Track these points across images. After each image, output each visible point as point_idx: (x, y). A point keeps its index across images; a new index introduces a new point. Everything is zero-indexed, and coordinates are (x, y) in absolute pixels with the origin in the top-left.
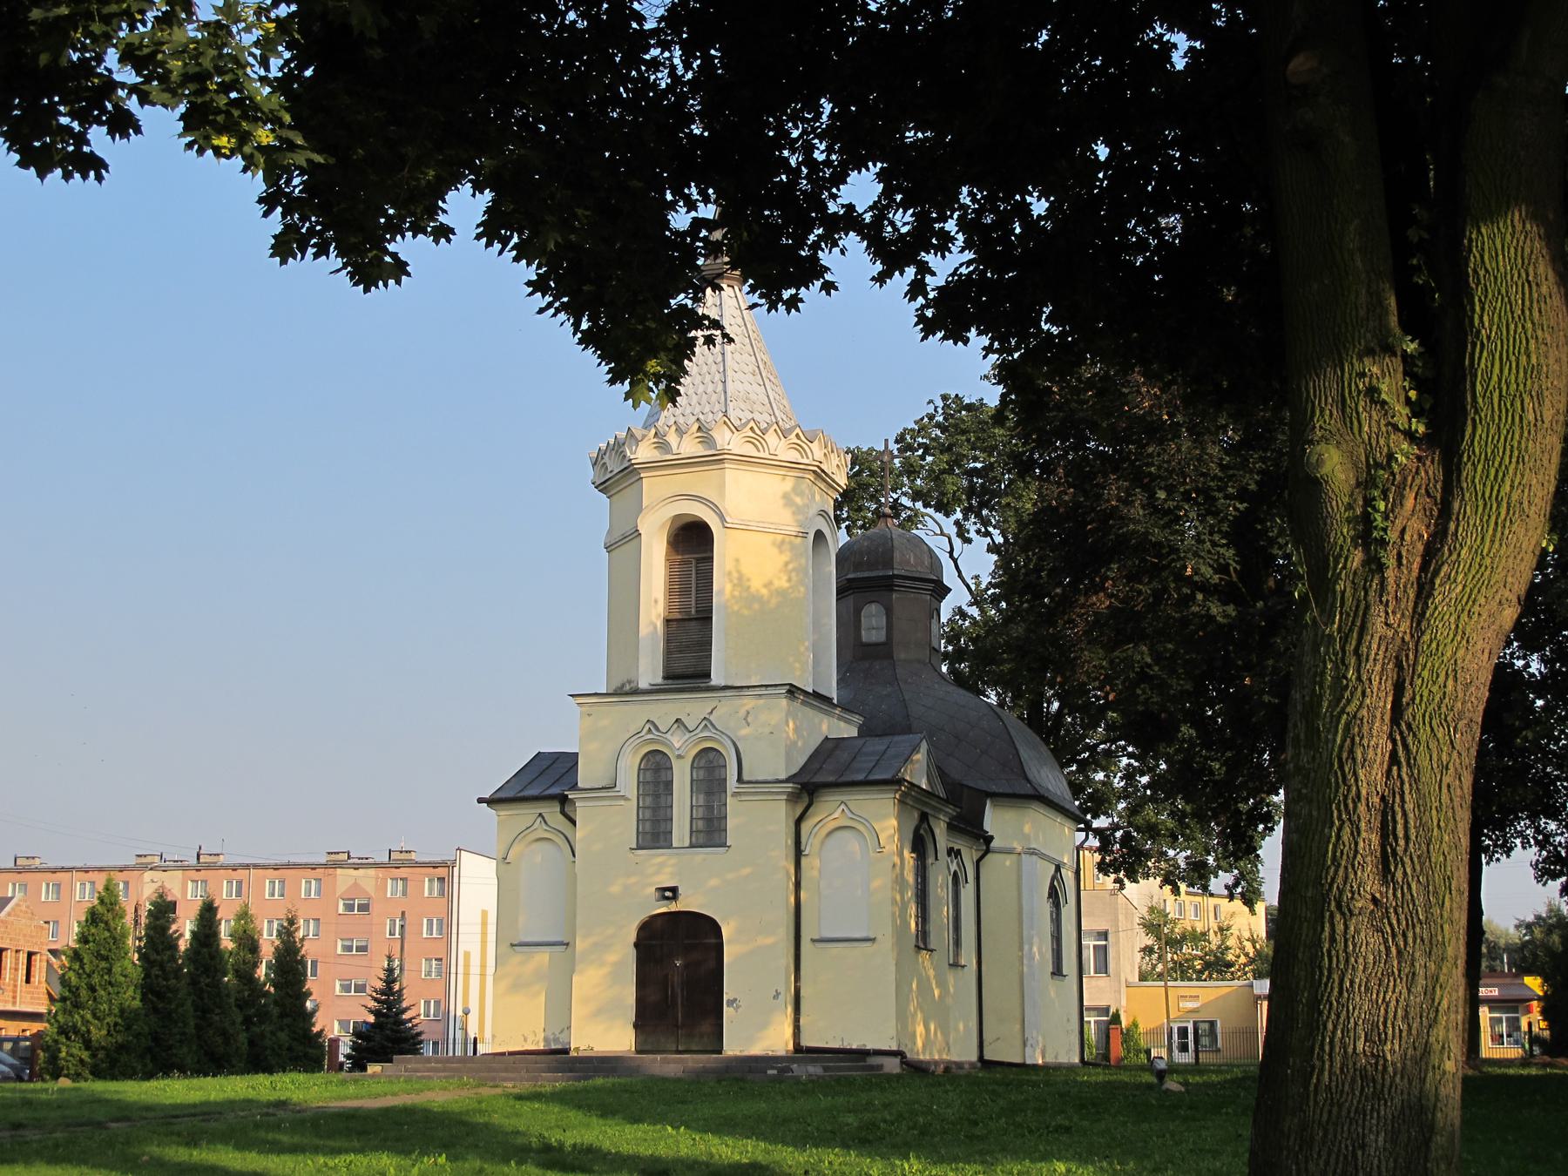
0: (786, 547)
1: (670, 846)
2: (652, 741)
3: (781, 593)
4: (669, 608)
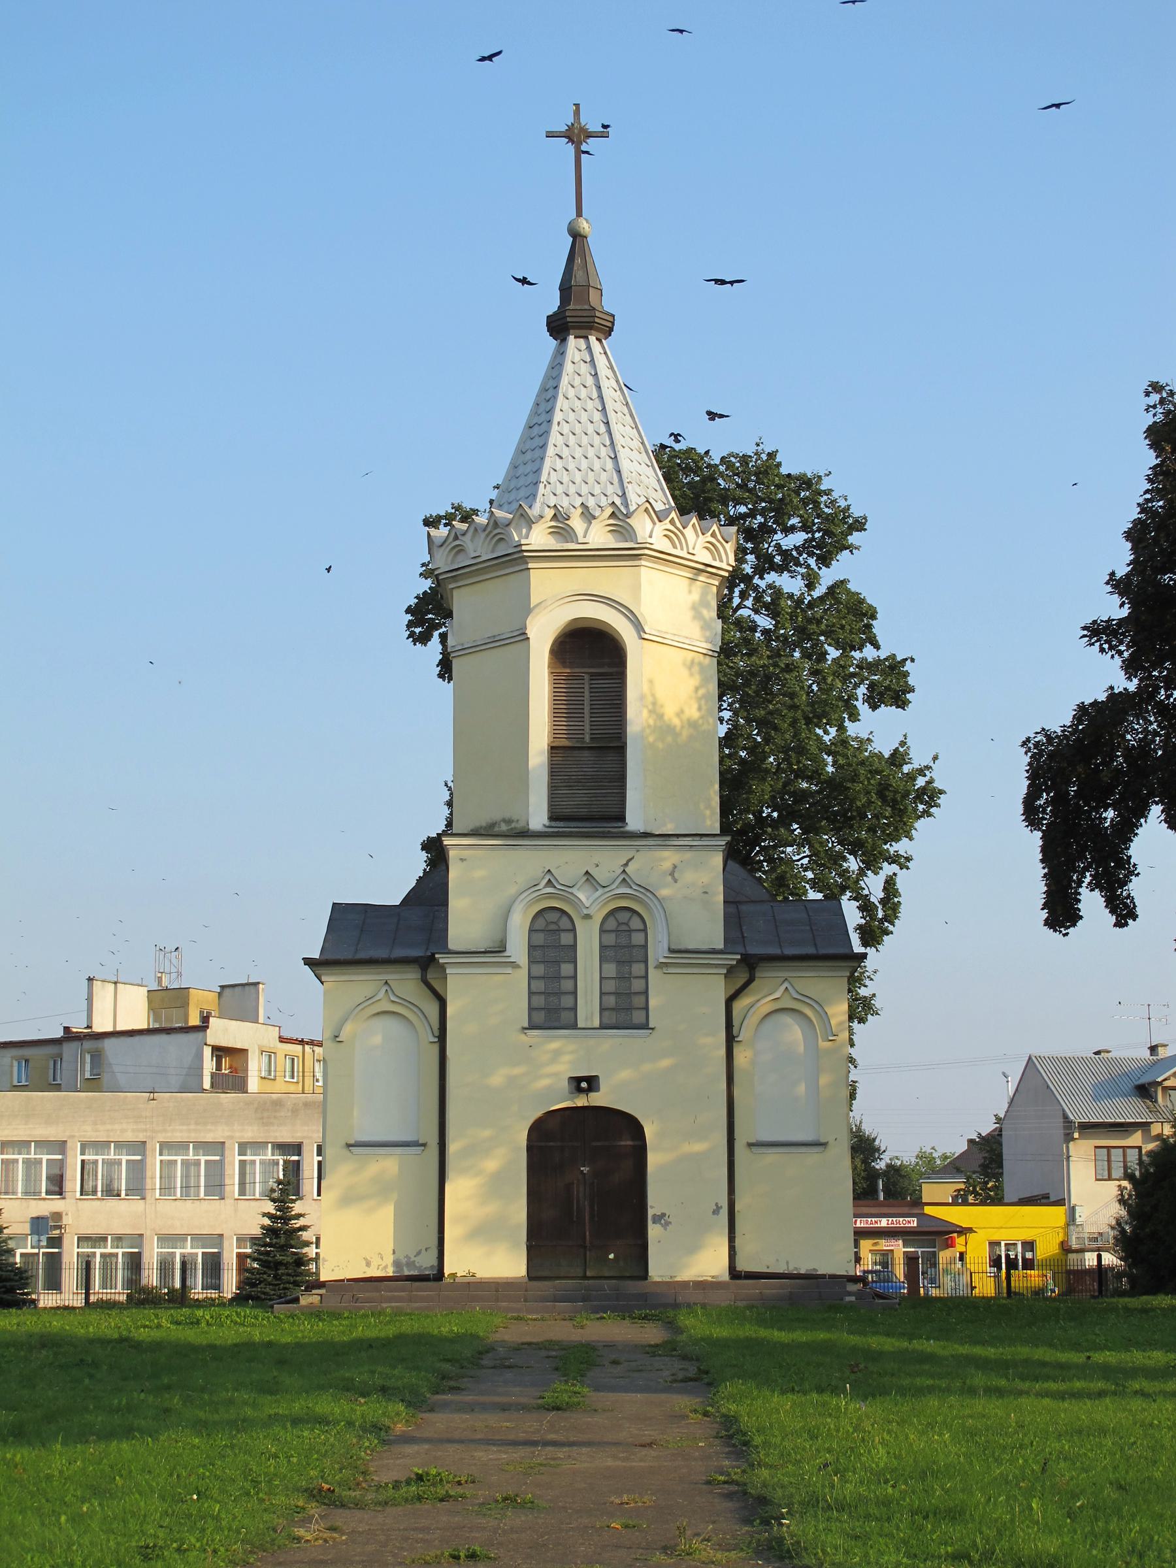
0: (696, 669)
1: (574, 1026)
2: (550, 896)
3: (692, 724)
4: (554, 734)
